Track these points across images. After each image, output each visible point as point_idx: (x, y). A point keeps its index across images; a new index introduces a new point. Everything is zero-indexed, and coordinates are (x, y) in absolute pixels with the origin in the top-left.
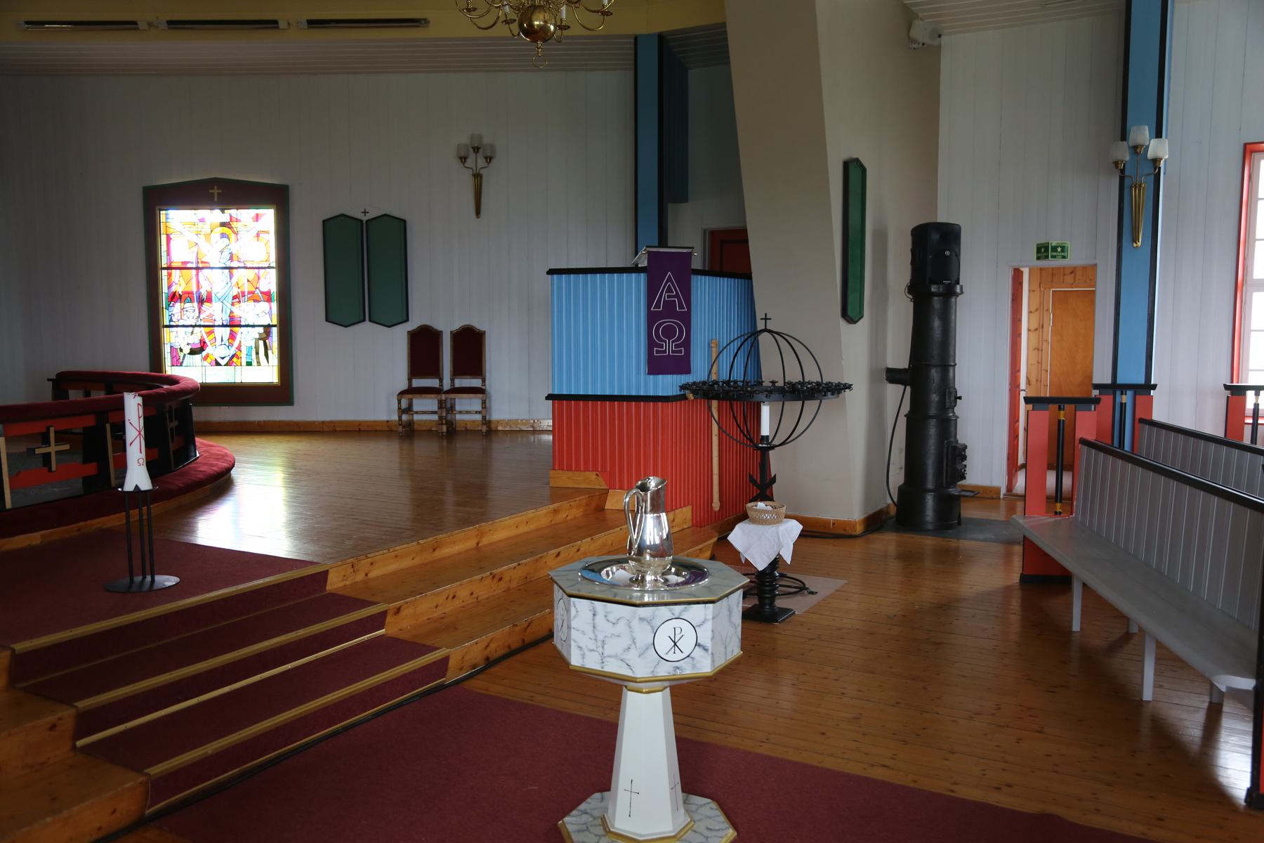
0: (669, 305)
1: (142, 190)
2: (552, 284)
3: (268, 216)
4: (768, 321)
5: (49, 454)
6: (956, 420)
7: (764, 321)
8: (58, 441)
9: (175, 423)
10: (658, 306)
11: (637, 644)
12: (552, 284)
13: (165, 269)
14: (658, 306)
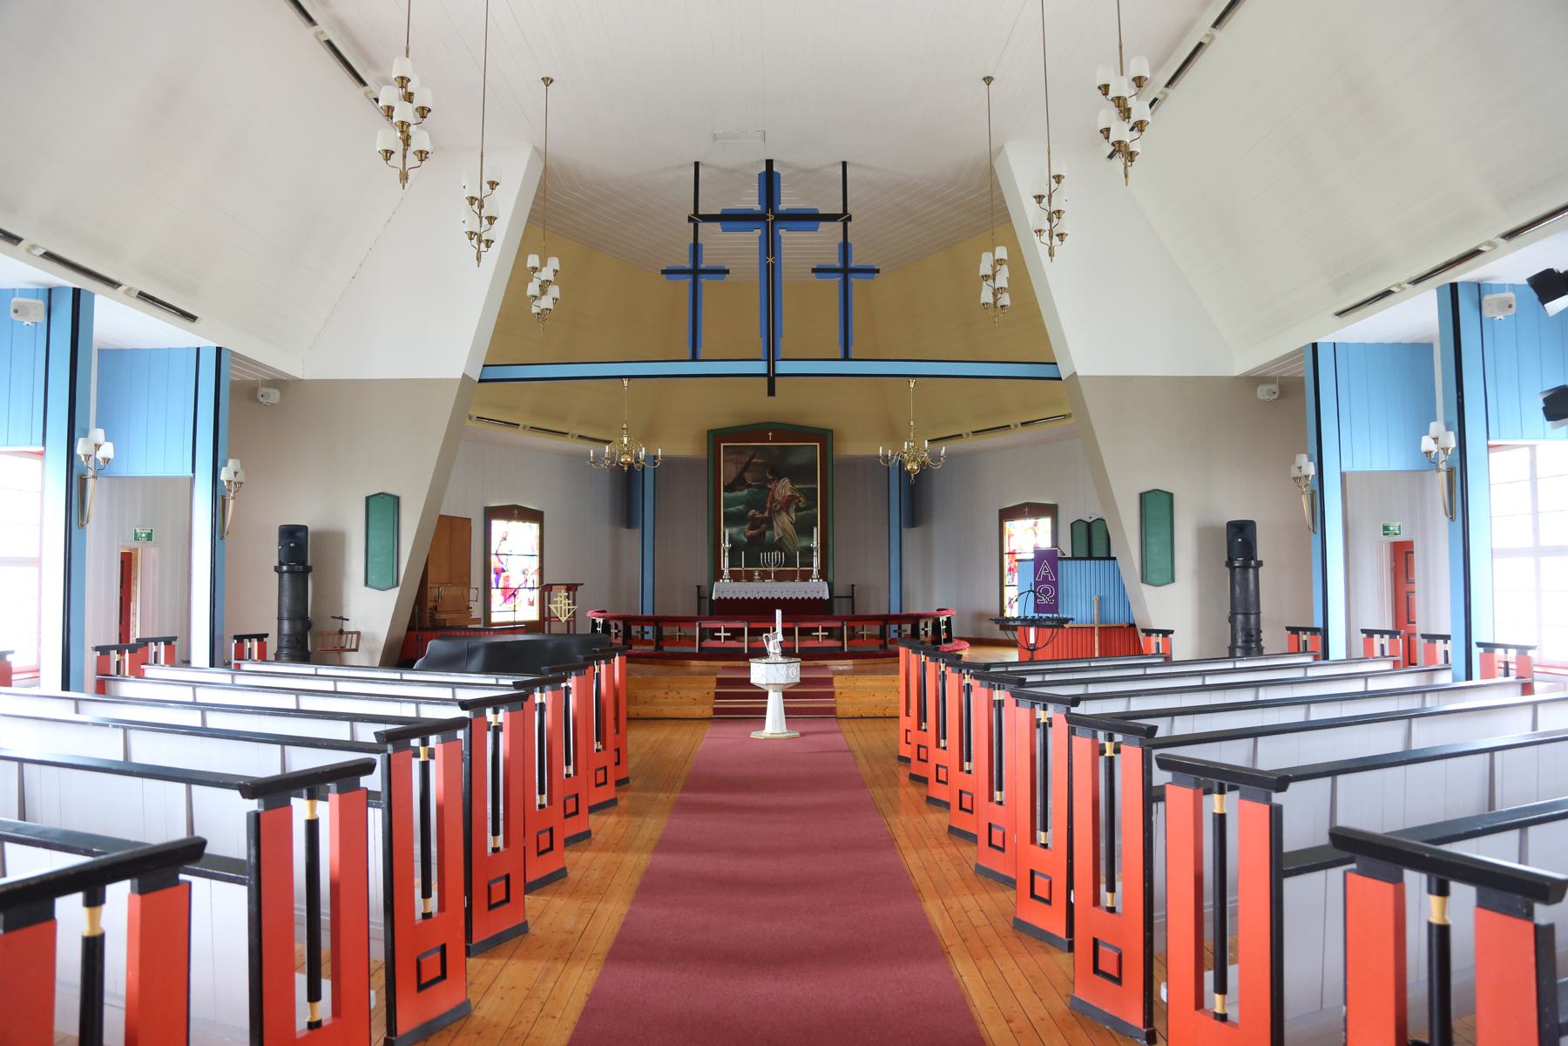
0: (1045, 577)
1: (483, 511)
2: (1420, 880)
3: (535, 527)
4: (854, 280)
5: (720, 632)
6: (281, 564)
7: (837, 280)
8: (822, 631)
9: (945, 627)
10: (1039, 578)
11: (1508, 655)
12: (1420, 880)
13: (900, 628)
14: (1039, 578)
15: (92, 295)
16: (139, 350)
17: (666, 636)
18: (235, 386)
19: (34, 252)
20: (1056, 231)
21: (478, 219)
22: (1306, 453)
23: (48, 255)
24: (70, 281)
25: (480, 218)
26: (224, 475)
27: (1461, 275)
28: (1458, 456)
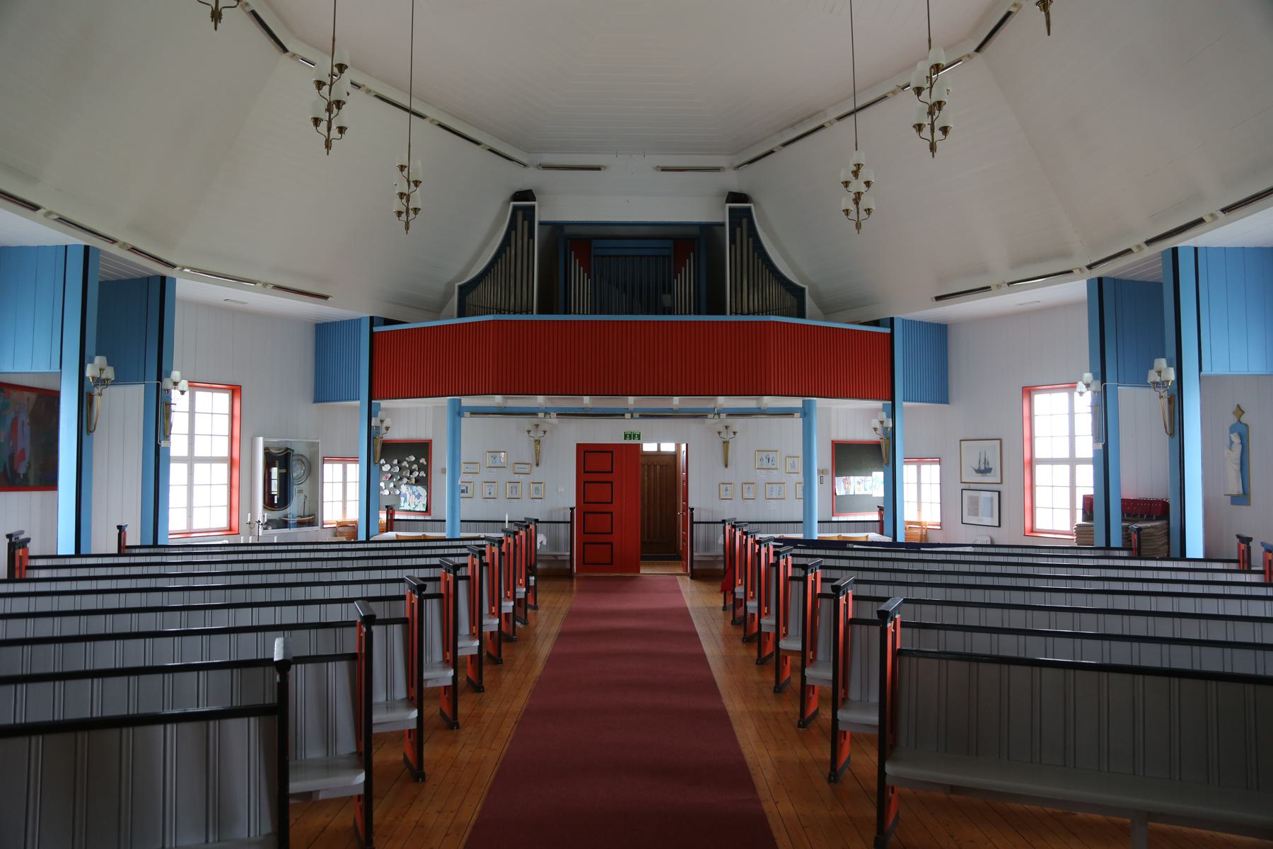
15: (173, 280)
16: (4, 247)
17: (285, 654)
18: (104, 285)
19: (50, 217)
20: (938, 125)
21: (407, 183)
22: (1164, 357)
23: (62, 220)
24: (81, 239)
25: (408, 181)
26: (90, 371)
27: (1185, 242)
28: (1176, 387)
